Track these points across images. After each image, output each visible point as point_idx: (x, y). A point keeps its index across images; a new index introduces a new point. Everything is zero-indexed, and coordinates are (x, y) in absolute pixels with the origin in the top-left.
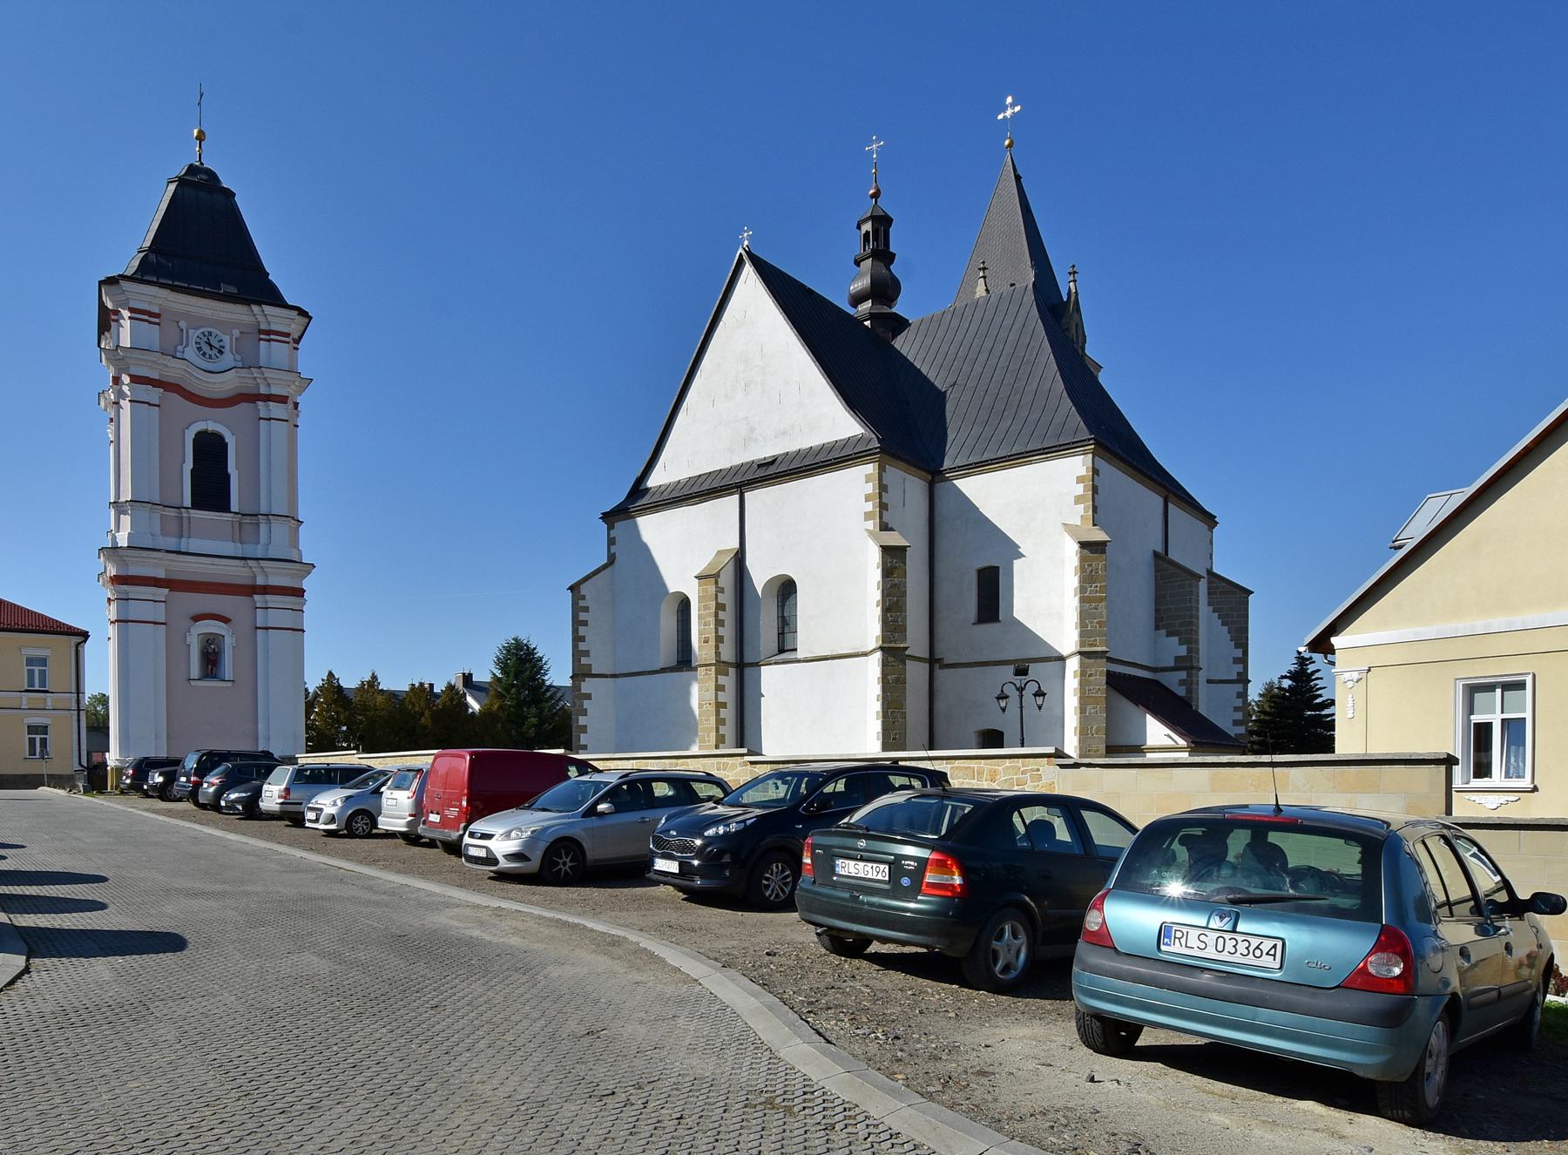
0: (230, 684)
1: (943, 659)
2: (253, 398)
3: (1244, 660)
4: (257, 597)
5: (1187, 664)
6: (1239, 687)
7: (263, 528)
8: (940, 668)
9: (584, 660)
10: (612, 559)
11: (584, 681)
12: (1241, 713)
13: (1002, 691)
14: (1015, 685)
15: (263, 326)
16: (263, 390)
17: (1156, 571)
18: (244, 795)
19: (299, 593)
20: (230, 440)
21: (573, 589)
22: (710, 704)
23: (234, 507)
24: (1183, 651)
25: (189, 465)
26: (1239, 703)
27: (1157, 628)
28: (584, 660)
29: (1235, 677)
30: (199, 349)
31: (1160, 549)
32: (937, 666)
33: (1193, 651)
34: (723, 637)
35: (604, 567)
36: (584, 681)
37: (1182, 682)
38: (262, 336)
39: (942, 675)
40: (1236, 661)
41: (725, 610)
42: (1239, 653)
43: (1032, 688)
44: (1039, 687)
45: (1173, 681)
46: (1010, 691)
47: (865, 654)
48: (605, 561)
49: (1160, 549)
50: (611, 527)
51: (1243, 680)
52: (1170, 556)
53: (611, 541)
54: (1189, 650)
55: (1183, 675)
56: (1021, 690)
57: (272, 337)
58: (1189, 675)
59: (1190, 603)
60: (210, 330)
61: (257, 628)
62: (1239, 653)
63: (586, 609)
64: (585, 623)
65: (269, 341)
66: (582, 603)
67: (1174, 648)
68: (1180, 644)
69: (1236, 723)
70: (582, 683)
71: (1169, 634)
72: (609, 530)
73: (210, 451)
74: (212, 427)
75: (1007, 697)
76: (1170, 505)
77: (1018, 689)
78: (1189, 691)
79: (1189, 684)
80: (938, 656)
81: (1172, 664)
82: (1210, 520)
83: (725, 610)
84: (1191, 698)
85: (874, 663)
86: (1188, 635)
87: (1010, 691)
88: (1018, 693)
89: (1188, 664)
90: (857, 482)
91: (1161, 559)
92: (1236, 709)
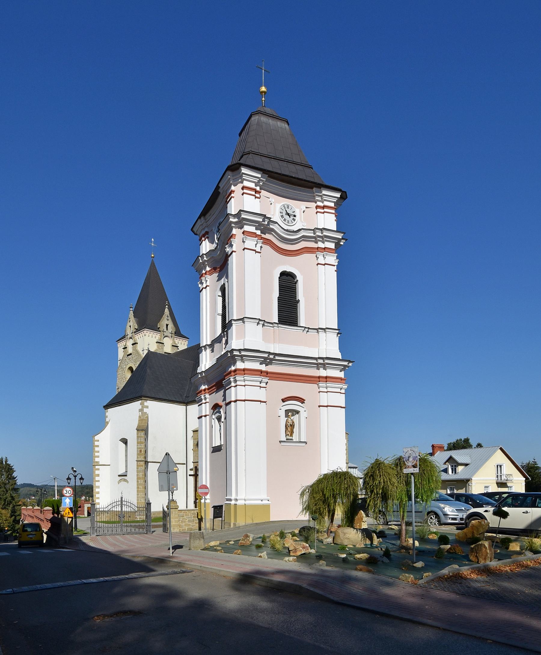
12: (96, 491)
13: (69, 477)
14: (73, 475)
23: (302, 321)
30: (282, 216)
38: (319, 210)
43: (79, 477)
44: (82, 477)
46: (72, 477)
56: (75, 477)
57: (326, 210)
74: (289, 269)
75: (83, 479)
77: (74, 476)
87: (72, 477)
88: (74, 478)
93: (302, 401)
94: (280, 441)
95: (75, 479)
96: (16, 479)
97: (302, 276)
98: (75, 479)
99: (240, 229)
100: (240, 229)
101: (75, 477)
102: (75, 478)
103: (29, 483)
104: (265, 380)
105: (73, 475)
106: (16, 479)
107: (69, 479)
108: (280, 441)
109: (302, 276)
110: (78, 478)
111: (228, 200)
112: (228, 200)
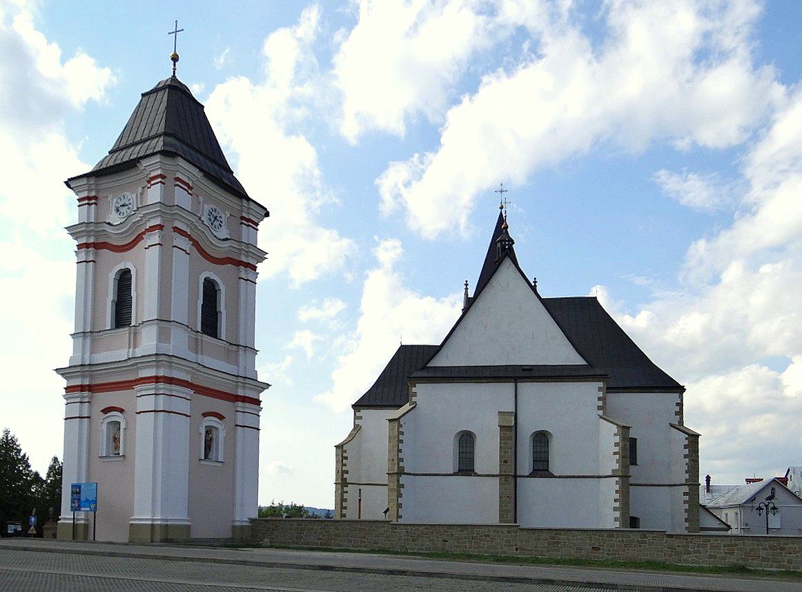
0: (220, 465)
2: (239, 263)
4: (240, 404)
7: (241, 352)
15: (244, 215)
16: (244, 259)
19: (258, 402)
20: (222, 287)
25: (201, 302)
40: (677, 413)
60: (215, 207)
61: (237, 425)
65: (248, 226)
73: (210, 290)
74: (213, 277)
93: (122, 411)
101: (767, 506)
104: (86, 393)
111: (152, 182)
112: (152, 182)
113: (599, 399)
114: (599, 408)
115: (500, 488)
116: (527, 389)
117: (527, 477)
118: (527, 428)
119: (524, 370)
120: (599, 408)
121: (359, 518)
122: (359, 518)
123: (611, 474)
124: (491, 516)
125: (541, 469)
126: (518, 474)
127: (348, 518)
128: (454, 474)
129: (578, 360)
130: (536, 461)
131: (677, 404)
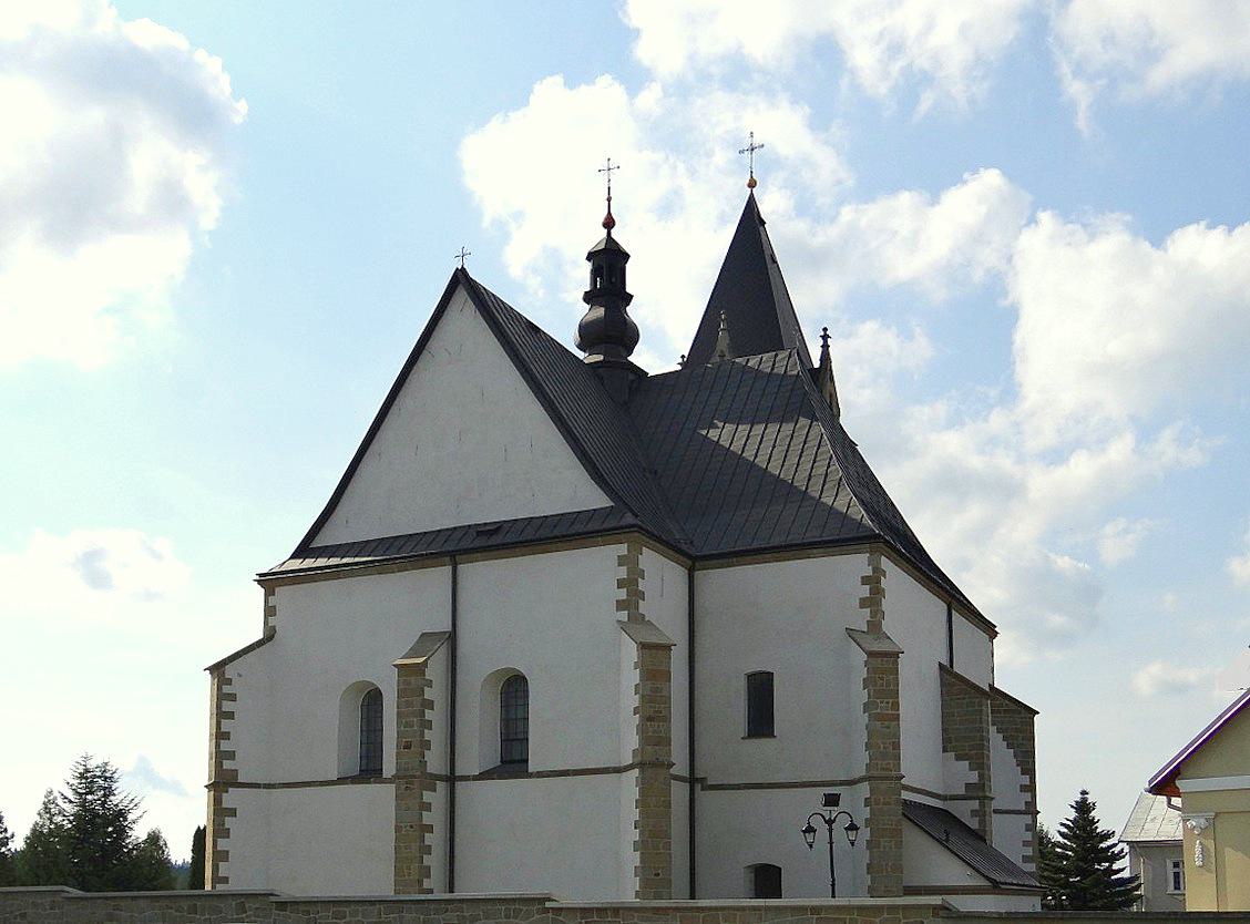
1: (705, 778)
3: (1031, 788)
5: (978, 791)
6: (1028, 819)
8: (702, 790)
9: (227, 765)
10: (270, 635)
11: (227, 792)
14: (823, 817)
17: (942, 686)
18: (867, 521)
21: (217, 670)
22: (412, 827)
24: (974, 777)
26: (1028, 836)
27: (945, 750)
28: (227, 765)
29: (1022, 807)
31: (945, 662)
32: (698, 787)
33: (984, 779)
34: (1022, 774)
35: (259, 644)
36: (227, 792)
37: (974, 813)
39: (708, 801)
40: (1024, 788)
41: (433, 709)
42: (1026, 780)
45: (964, 811)
46: (818, 823)
47: (618, 770)
48: (259, 635)
49: (945, 662)
50: (269, 593)
51: (1031, 810)
52: (955, 670)
53: (269, 611)
54: (981, 776)
55: (975, 804)
56: (830, 822)
58: (982, 805)
59: (981, 723)
62: (1026, 780)
63: (233, 697)
64: (230, 715)
66: (226, 689)
67: (964, 773)
68: (971, 769)
69: (1026, 859)
70: (224, 794)
71: (958, 758)
72: (266, 596)
76: (955, 615)
77: (826, 822)
78: (983, 822)
79: (980, 814)
80: (699, 774)
81: (962, 791)
82: (990, 630)
83: (433, 709)
84: (985, 831)
85: (630, 784)
86: (979, 762)
87: (818, 823)
89: (981, 794)
90: (599, 565)
91: (946, 670)
92: (1026, 844)
94: (461, 279)
95: (831, 830)
96: (1070, 823)
97: (640, 567)
98: (831, 830)
99: (1072, 814)
100: (1072, 814)
101: (830, 822)
102: (830, 826)
103: (1008, 747)
105: (823, 817)
106: (1070, 823)
107: (810, 830)
108: (461, 279)
109: (640, 567)
110: (839, 827)
113: (621, 584)
114: (621, 605)
115: (398, 808)
116: (477, 574)
117: (476, 778)
118: (481, 661)
119: (479, 533)
120: (621, 605)
121: (995, 811)
122: (995, 811)
123: (964, 793)
124: (377, 880)
125: (512, 761)
126: (458, 773)
127: (232, 887)
128: (341, 781)
129: (595, 499)
130: (508, 740)
131: (1024, 788)
